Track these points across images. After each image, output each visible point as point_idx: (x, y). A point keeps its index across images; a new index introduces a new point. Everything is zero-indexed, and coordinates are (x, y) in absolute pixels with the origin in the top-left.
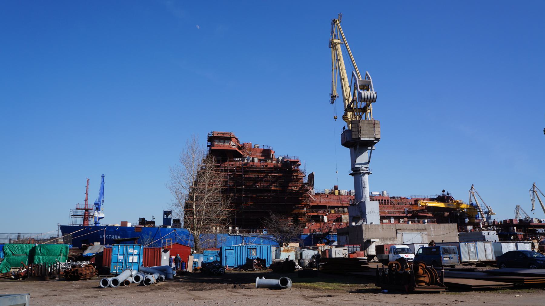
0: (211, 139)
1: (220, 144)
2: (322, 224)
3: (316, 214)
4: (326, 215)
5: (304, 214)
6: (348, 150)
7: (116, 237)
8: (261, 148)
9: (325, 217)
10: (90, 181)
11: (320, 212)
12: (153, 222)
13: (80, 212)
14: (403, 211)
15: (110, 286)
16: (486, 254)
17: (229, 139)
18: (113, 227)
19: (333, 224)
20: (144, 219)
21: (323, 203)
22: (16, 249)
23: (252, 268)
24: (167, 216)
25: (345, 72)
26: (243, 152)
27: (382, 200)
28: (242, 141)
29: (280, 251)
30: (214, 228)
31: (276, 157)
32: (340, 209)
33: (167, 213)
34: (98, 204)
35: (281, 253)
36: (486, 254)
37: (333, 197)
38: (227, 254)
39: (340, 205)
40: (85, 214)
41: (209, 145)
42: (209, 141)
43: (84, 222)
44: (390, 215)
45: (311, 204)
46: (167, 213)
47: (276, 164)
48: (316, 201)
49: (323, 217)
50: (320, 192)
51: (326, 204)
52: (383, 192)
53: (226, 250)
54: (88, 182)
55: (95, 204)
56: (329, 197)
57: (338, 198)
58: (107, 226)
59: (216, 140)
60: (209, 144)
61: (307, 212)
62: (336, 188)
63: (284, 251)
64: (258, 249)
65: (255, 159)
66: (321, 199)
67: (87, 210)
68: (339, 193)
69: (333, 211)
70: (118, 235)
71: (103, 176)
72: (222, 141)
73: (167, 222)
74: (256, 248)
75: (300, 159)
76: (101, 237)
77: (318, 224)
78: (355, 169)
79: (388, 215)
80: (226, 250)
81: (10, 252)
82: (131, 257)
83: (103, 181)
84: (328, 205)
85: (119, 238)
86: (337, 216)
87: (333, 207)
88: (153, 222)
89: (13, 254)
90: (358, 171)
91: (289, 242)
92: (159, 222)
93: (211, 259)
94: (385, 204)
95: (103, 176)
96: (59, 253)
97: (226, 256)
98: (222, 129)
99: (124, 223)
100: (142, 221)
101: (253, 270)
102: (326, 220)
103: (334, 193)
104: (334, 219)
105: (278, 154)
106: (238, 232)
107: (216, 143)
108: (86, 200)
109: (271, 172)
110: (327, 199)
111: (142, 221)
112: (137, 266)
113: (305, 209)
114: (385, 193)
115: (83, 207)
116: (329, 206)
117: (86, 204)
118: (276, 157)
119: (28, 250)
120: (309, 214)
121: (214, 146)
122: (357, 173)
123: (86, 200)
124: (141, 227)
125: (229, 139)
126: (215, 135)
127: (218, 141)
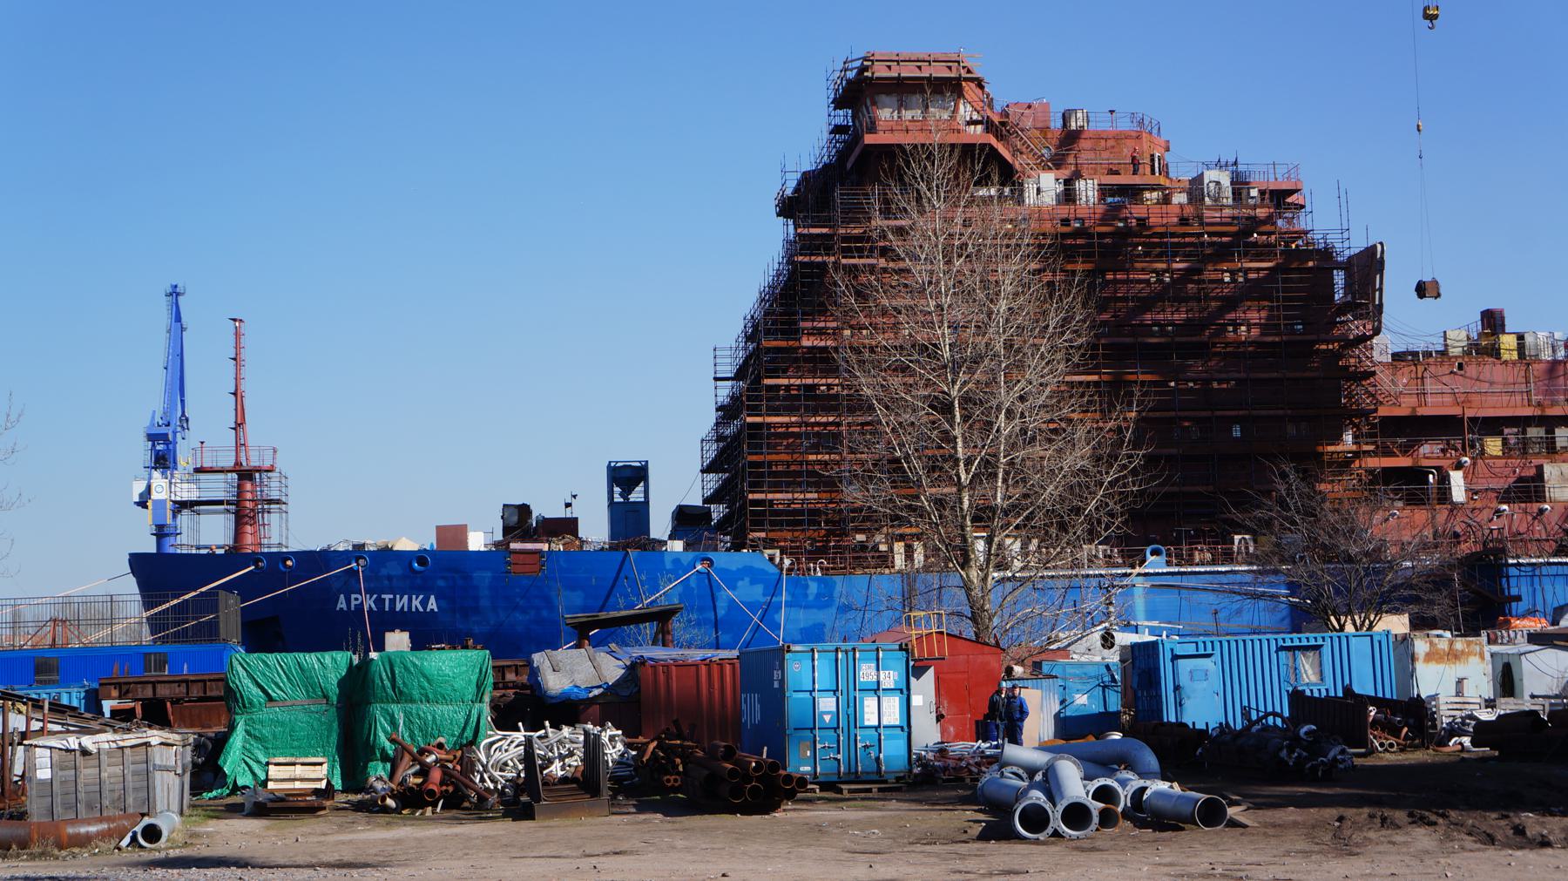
0: (858, 92)
1: (907, 115)
2: (1442, 514)
3: (1404, 462)
4: (1459, 466)
5: (1343, 464)
7: (416, 603)
9: (1457, 479)
10: (244, 328)
11: (1425, 449)
12: (567, 527)
13: (218, 487)
15: (1056, 834)
17: (950, 88)
18: (386, 554)
19: (1498, 512)
20: (524, 510)
21: (1437, 405)
22: (282, 680)
23: (1362, 741)
24: (626, 492)
26: (1016, 152)
28: (1005, 92)
29: (1413, 658)
30: (899, 547)
31: (1182, 172)
32: (1534, 432)
33: (627, 477)
34: (164, 437)
35: (1420, 667)
37: (1491, 370)
38: (1184, 680)
39: (1528, 412)
40: (240, 490)
41: (840, 121)
42: (839, 103)
43: (238, 534)
45: (1383, 411)
46: (627, 477)
47: (1189, 211)
48: (1398, 396)
49: (1444, 479)
50: (1420, 346)
51: (1456, 411)
53: (1175, 658)
54: (238, 334)
55: (152, 438)
56: (1471, 370)
57: (1519, 372)
58: (359, 548)
59: (883, 98)
60: (843, 117)
61: (1357, 455)
62: (1493, 321)
63: (1429, 657)
64: (1326, 650)
65: (1080, 185)
66: (1430, 386)
67: (245, 475)
68: (1521, 348)
69: (1493, 446)
70: (424, 589)
71: (175, 293)
72: (917, 99)
73: (629, 520)
74: (1317, 648)
76: (342, 604)
77: (1421, 515)
80: (1175, 658)
81: (255, 690)
82: (870, 704)
83: (178, 318)
84: (1469, 413)
85: (432, 604)
86: (1521, 468)
87: (1492, 426)
88: (567, 527)
89: (270, 699)
91: (1379, 612)
92: (595, 529)
93: (1081, 700)
95: (175, 293)
96: (472, 689)
97: (1177, 688)
98: (901, 42)
99: (453, 534)
100: (519, 521)
101: (1372, 751)
102: (1458, 493)
103: (1494, 352)
104: (1501, 484)
106: (1018, 564)
107: (885, 114)
108: (239, 425)
109: (1222, 253)
110: (1460, 385)
111: (519, 521)
112: (903, 743)
113: (1348, 437)
115: (229, 462)
116: (1473, 420)
117: (239, 445)
118: (1182, 172)
119: (335, 682)
120: (1374, 463)
121: (872, 129)
123: (239, 425)
124: (540, 552)
125: (950, 88)
126: (880, 71)
127: (893, 99)
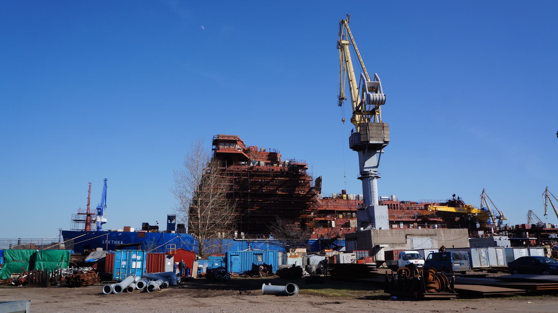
0: (216, 142)
1: (226, 147)
2: (330, 229)
3: (323, 219)
4: (334, 220)
5: (311, 219)
6: (356, 153)
7: (118, 242)
8: (268, 151)
9: (333, 222)
10: (92, 185)
11: (328, 216)
12: (157, 228)
13: (82, 217)
14: (412, 215)
15: (113, 293)
16: (497, 260)
17: (234, 142)
18: (116, 232)
19: (341, 230)
20: (147, 224)
21: (330, 208)
22: (17, 255)
23: (258, 274)
24: (171, 221)
25: (353, 73)
26: (249, 155)
27: (391, 205)
28: (248, 144)
29: (287, 257)
30: (219, 234)
31: (282, 161)
32: (348, 214)
33: (171, 218)
34: (100, 209)
35: (288, 258)
36: (497, 260)
37: (341, 201)
38: (233, 260)
39: (348, 210)
40: (87, 218)
41: (214, 148)
42: (214, 144)
43: (86, 227)
44: (399, 220)
45: (319, 209)
46: (171, 218)
47: (282, 168)
48: (323, 206)
49: (331, 222)
50: (328, 196)
51: (333, 209)
52: (392, 196)
53: (231, 256)
54: (90, 186)
55: (98, 209)
56: (337, 201)
57: (346, 202)
58: (110, 231)
59: (221, 144)
60: (214, 147)
61: (314, 217)
62: (344, 192)
63: (290, 257)
64: (264, 255)
65: (261, 162)
66: (329, 204)
67: (89, 215)
68: (347, 197)
69: (341, 216)
70: (120, 240)
71: (105, 180)
72: (227, 144)
73: (171, 227)
74: (262, 254)
75: (307, 162)
76: (103, 242)
77: (326, 230)
78: (363, 173)
79: (398, 220)
80: (231, 256)
81: (10, 258)
82: (134, 263)
83: (106, 185)
84: (336, 210)
85: (122, 243)
86: (345, 221)
87: (341, 212)
88: (157, 228)
89: (13, 260)
90: (366, 175)
91: (296, 248)
92: (163, 228)
93: (217, 264)
94: (394, 209)
95: (105, 180)
96: (60, 259)
97: (231, 262)
98: (227, 132)
99: (127, 229)
100: (146, 226)
101: (259, 276)
102: (333, 225)
103: (342, 198)
104: (342, 224)
105: (285, 158)
106: (243, 237)
107: (221, 147)
108: (88, 205)
109: (277, 176)
110: (335, 204)
111: (146, 226)
112: (141, 272)
113: (312, 214)
114: (394, 197)
115: (85, 212)
116: (337, 211)
117: (88, 209)
118: (282, 161)
119: (29, 256)
120: (317, 219)
121: (219, 150)
122: (365, 177)
123: (88, 205)
124: (145, 233)
125: (234, 142)
126: (220, 138)
127: (223, 144)
